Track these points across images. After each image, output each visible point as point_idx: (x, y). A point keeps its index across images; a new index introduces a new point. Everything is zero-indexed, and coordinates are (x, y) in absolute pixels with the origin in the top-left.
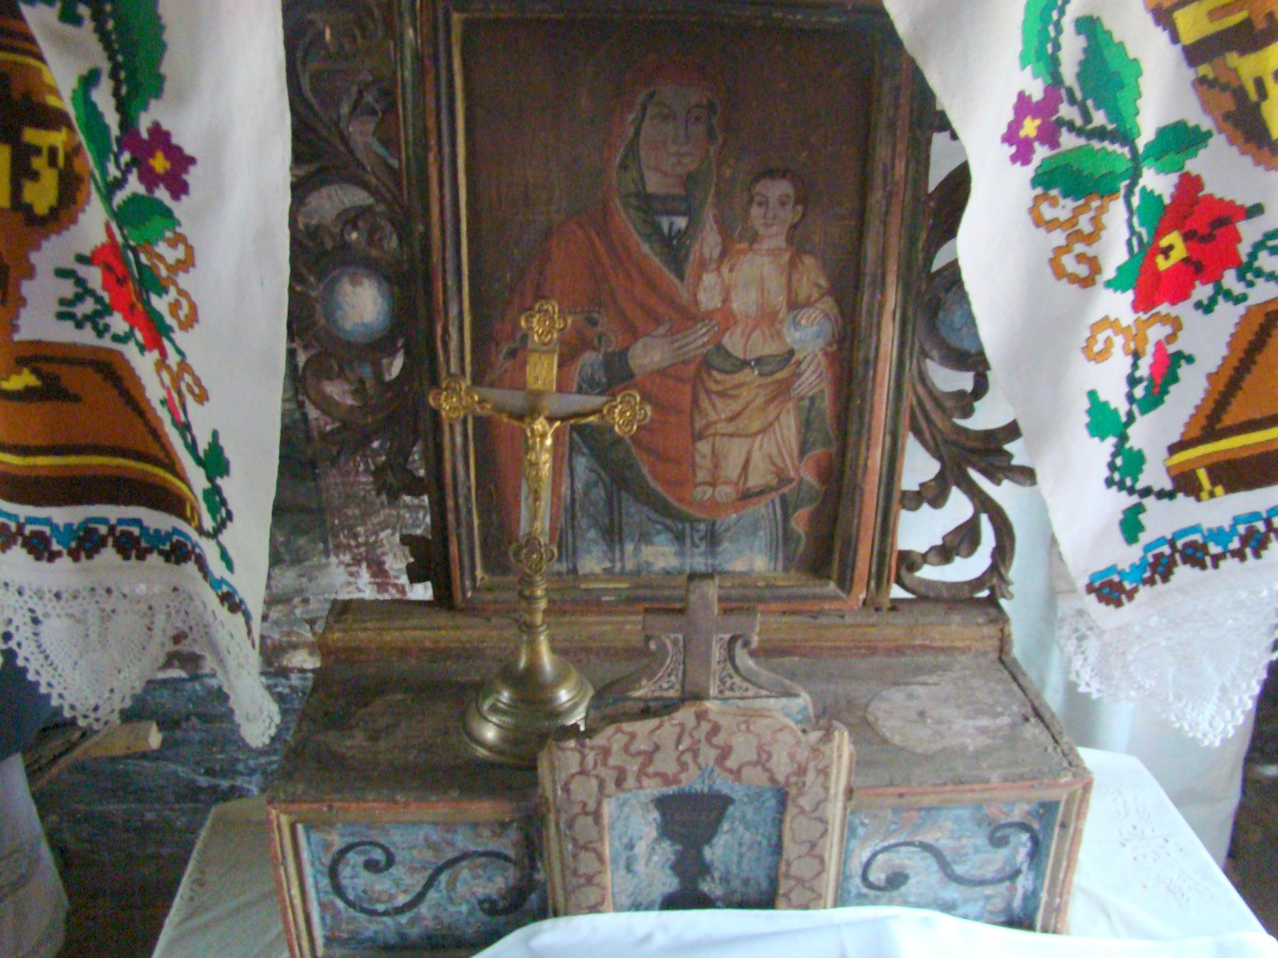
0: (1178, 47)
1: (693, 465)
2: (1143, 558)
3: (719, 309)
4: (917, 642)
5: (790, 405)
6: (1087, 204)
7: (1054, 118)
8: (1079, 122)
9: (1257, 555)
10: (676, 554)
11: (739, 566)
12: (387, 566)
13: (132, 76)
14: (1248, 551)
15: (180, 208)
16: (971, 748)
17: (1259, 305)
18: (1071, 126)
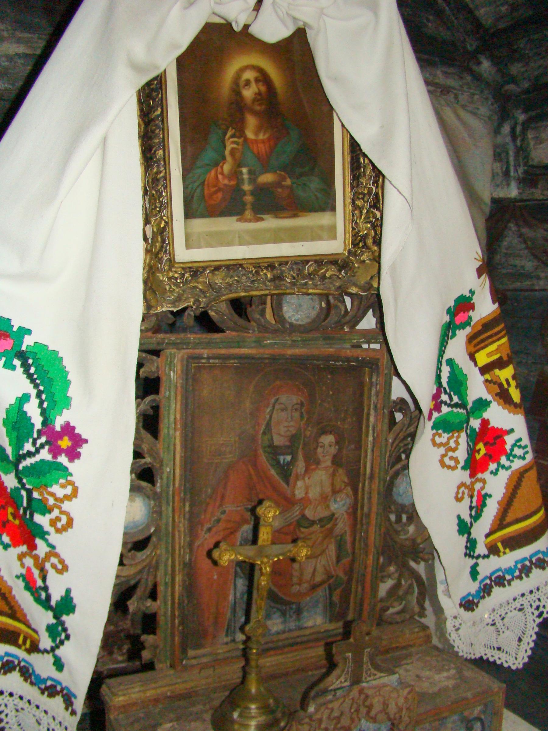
0: (477, 368)
1: (292, 575)
2: (480, 587)
3: (304, 498)
4: (394, 646)
5: (333, 540)
6: (453, 435)
7: (439, 400)
8: (448, 401)
9: (527, 576)
10: (282, 623)
11: (310, 623)
14: (523, 575)
16: (450, 686)
17: (517, 470)
18: (445, 403)
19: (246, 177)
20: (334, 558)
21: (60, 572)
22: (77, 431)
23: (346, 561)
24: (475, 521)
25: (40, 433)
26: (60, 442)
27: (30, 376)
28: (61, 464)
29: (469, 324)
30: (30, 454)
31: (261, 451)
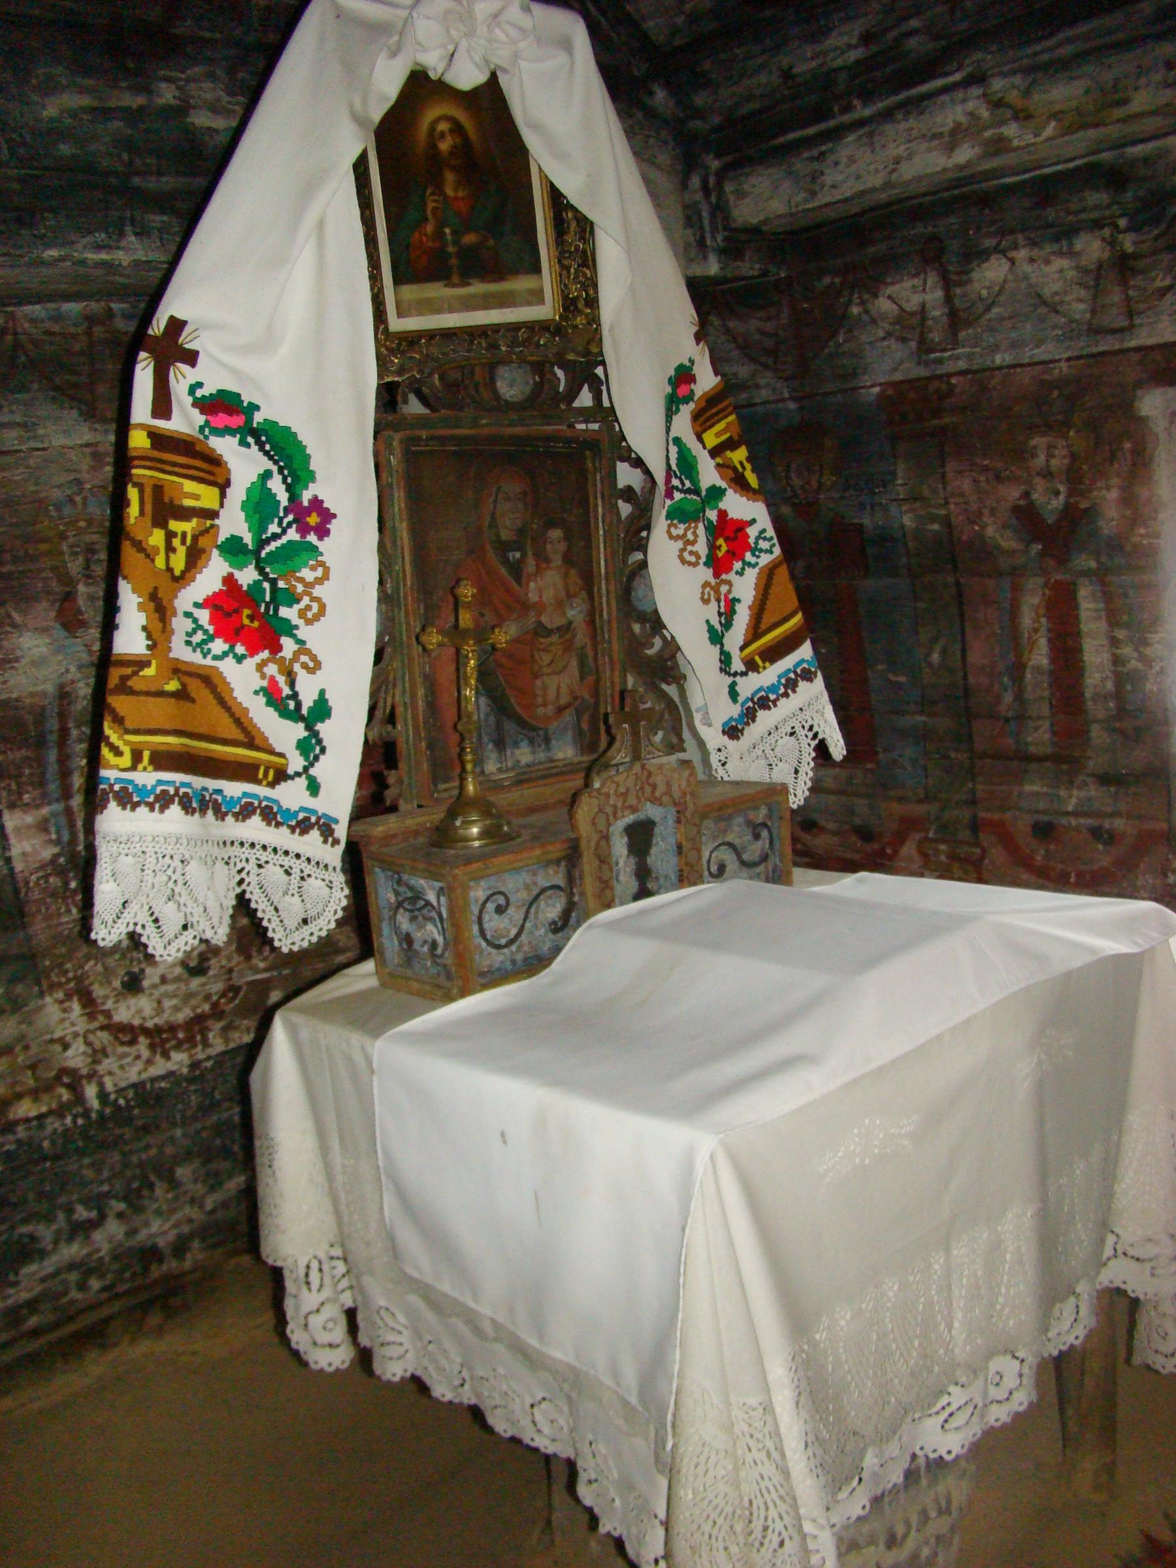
9: (794, 691)
11: (560, 755)
12: (94, 994)
13: (293, 474)
15: (323, 545)
18: (677, 489)
19: (449, 238)
20: (577, 674)
21: (311, 671)
22: (325, 505)
23: (590, 679)
24: (727, 630)
25: (287, 510)
26: (308, 519)
27: (266, 453)
28: (310, 543)
29: (692, 399)
30: (275, 537)
31: (488, 547)
